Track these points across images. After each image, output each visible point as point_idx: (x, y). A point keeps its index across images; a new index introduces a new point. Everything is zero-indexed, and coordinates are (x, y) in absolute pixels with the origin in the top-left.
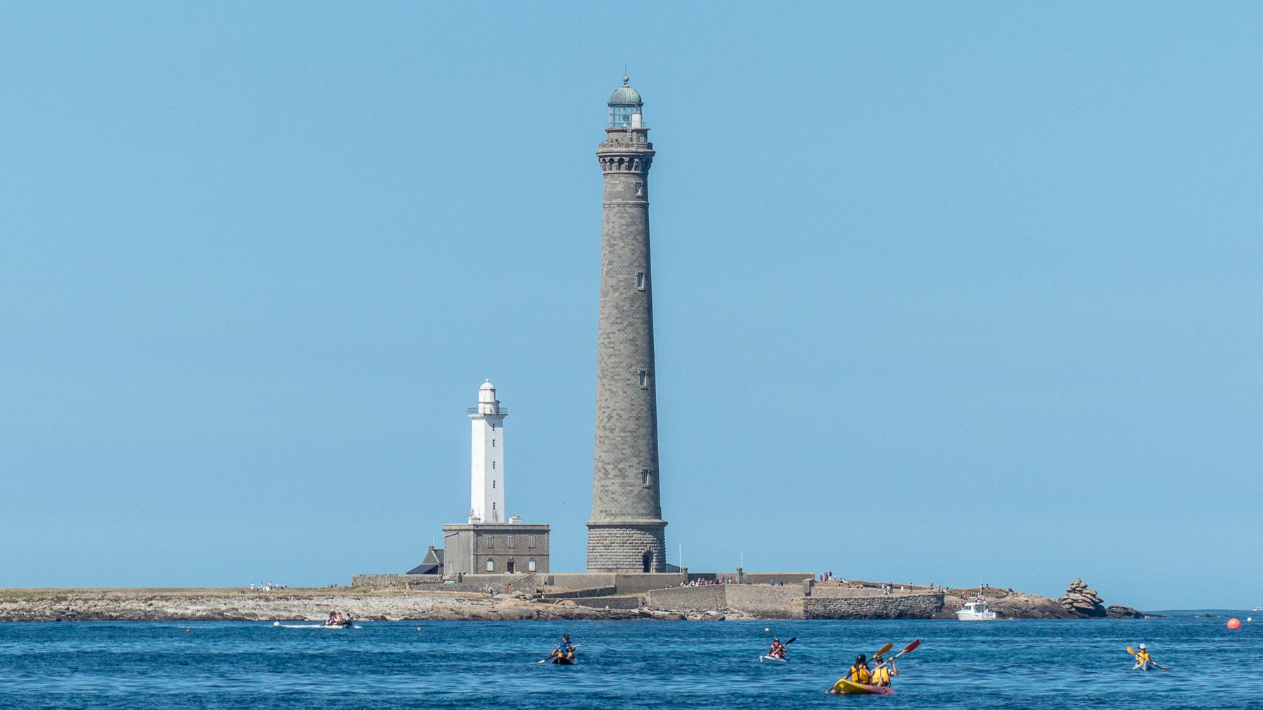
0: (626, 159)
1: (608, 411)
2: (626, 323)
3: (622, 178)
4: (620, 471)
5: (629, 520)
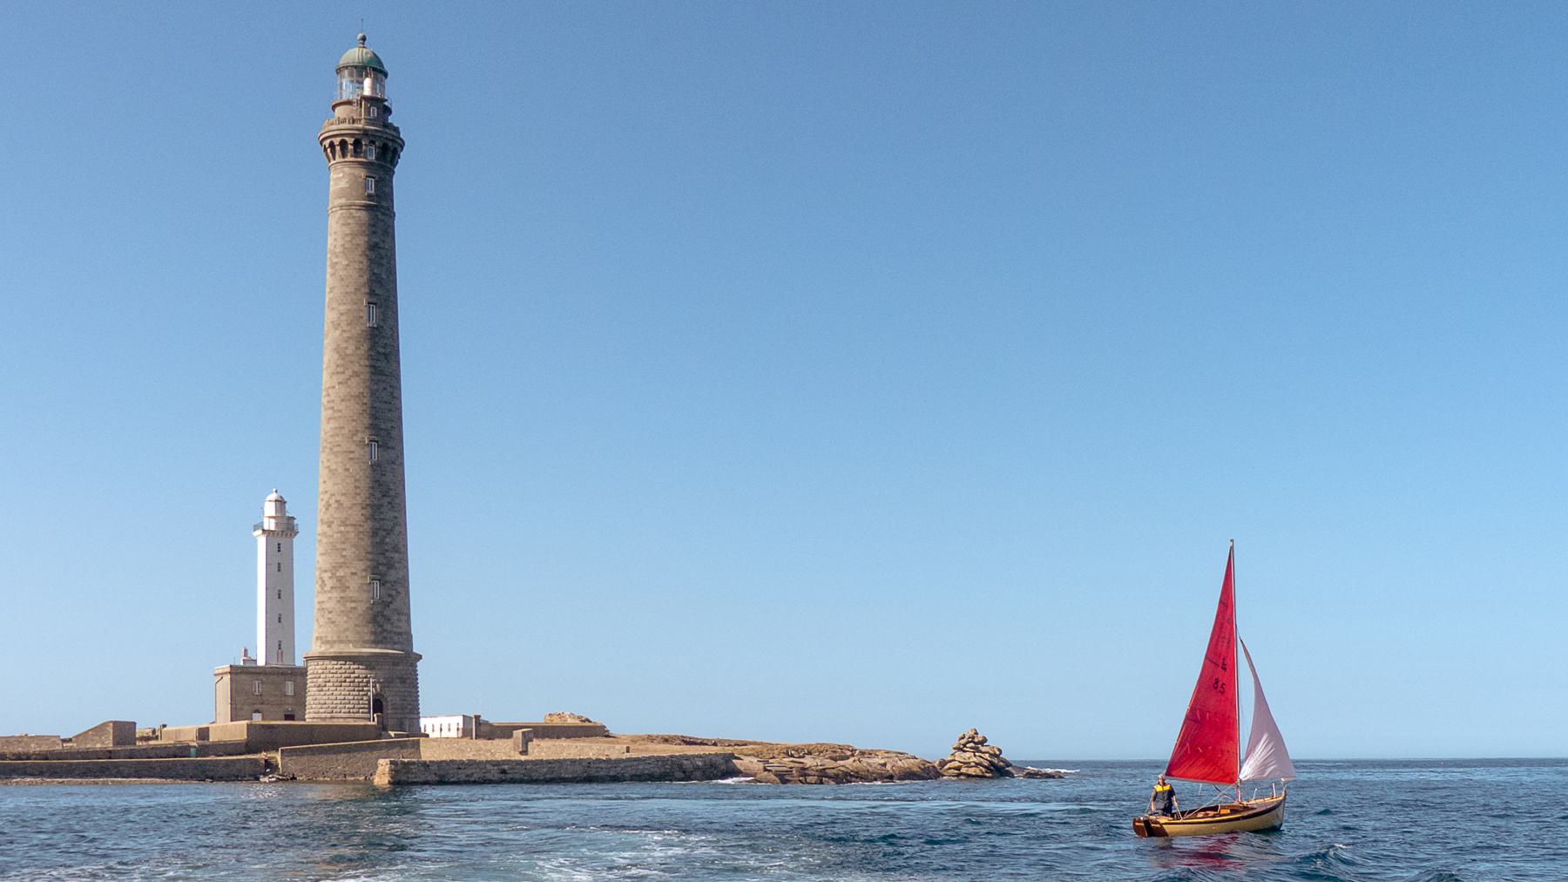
0: (350, 140)
1: (326, 497)
2: (349, 373)
3: (347, 170)
4: (340, 580)
5: (351, 649)
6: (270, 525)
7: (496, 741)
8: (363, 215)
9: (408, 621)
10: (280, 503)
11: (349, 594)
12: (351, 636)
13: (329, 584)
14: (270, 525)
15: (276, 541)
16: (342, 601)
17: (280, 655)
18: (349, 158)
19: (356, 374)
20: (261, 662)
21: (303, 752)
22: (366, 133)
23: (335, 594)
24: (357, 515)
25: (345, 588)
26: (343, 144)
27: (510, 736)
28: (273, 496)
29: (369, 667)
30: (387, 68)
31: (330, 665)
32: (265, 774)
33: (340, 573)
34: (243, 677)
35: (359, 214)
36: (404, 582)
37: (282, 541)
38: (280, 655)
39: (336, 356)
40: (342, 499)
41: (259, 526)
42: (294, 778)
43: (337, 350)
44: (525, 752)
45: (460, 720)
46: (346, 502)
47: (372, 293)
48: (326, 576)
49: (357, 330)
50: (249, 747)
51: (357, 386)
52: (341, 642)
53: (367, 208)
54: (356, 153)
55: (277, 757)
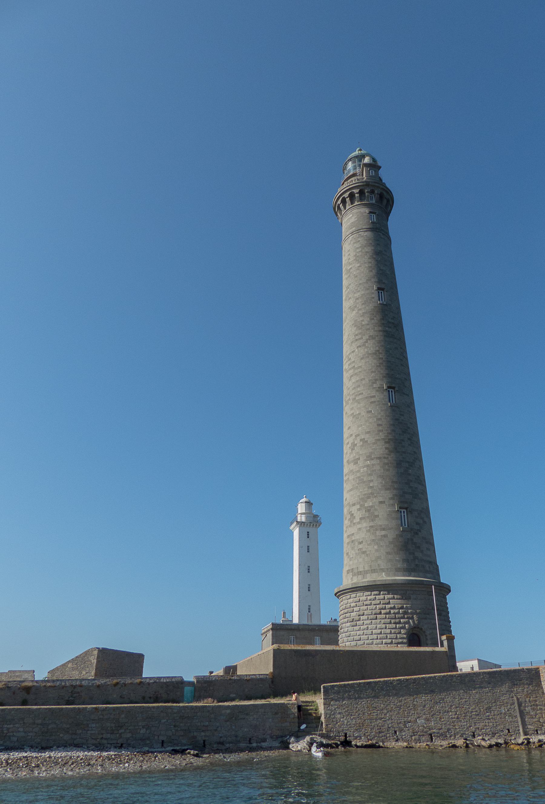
0: (356, 191)
2: (366, 337)
4: (368, 510)
5: (383, 577)
6: (302, 518)
8: (368, 234)
10: (309, 504)
12: (383, 564)
13: (358, 516)
14: (302, 518)
16: (372, 529)
17: (310, 617)
18: (356, 203)
21: (358, 693)
23: (364, 524)
24: (380, 449)
26: (352, 196)
29: (405, 596)
30: (379, 164)
31: (363, 596)
32: (299, 736)
33: (368, 504)
34: (282, 633)
35: (366, 233)
36: (426, 512)
37: (311, 530)
38: (310, 617)
42: (346, 743)
43: (355, 325)
45: (477, 661)
46: (370, 439)
47: (380, 281)
49: (371, 306)
50: (276, 685)
51: (372, 346)
52: (374, 571)
53: (371, 229)
54: (361, 199)
55: (318, 702)
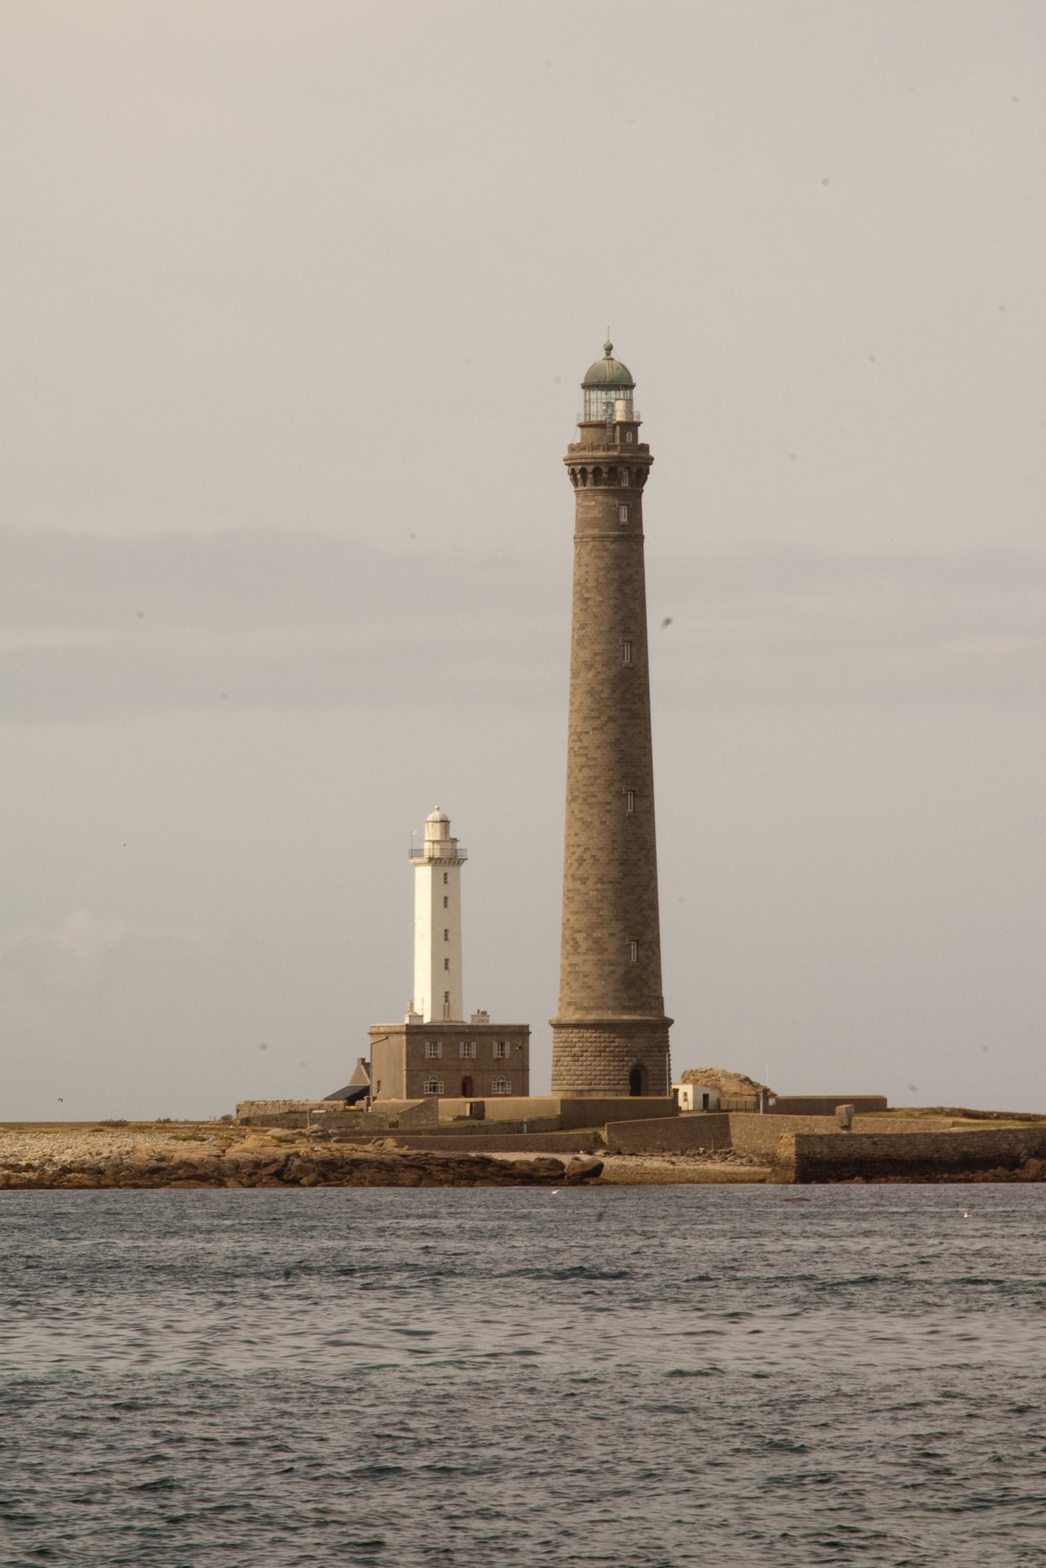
2: (604, 718)
3: (600, 498)
4: (596, 941)
5: (608, 1016)
7: (381, 1188)
9: (659, 984)
10: (445, 822)
11: (606, 956)
15: (442, 870)
16: (600, 963)
19: (611, 719)
20: (427, 1020)
22: (620, 460)
23: (591, 957)
25: (602, 951)
27: (832, 1113)
28: (436, 815)
33: (597, 934)
37: (449, 870)
39: (589, 699)
40: (599, 854)
41: (416, 853)
44: (847, 1127)
48: (580, 937)
